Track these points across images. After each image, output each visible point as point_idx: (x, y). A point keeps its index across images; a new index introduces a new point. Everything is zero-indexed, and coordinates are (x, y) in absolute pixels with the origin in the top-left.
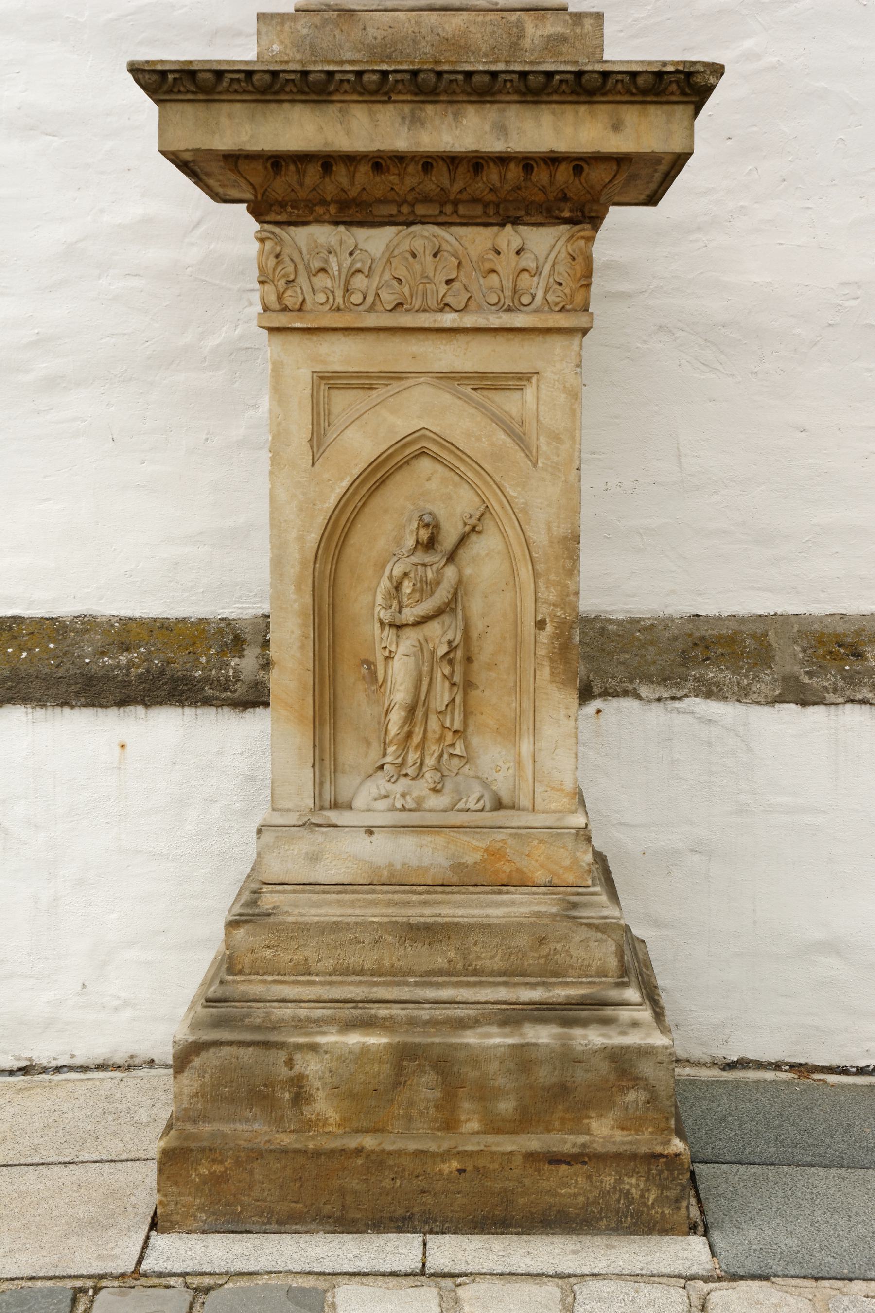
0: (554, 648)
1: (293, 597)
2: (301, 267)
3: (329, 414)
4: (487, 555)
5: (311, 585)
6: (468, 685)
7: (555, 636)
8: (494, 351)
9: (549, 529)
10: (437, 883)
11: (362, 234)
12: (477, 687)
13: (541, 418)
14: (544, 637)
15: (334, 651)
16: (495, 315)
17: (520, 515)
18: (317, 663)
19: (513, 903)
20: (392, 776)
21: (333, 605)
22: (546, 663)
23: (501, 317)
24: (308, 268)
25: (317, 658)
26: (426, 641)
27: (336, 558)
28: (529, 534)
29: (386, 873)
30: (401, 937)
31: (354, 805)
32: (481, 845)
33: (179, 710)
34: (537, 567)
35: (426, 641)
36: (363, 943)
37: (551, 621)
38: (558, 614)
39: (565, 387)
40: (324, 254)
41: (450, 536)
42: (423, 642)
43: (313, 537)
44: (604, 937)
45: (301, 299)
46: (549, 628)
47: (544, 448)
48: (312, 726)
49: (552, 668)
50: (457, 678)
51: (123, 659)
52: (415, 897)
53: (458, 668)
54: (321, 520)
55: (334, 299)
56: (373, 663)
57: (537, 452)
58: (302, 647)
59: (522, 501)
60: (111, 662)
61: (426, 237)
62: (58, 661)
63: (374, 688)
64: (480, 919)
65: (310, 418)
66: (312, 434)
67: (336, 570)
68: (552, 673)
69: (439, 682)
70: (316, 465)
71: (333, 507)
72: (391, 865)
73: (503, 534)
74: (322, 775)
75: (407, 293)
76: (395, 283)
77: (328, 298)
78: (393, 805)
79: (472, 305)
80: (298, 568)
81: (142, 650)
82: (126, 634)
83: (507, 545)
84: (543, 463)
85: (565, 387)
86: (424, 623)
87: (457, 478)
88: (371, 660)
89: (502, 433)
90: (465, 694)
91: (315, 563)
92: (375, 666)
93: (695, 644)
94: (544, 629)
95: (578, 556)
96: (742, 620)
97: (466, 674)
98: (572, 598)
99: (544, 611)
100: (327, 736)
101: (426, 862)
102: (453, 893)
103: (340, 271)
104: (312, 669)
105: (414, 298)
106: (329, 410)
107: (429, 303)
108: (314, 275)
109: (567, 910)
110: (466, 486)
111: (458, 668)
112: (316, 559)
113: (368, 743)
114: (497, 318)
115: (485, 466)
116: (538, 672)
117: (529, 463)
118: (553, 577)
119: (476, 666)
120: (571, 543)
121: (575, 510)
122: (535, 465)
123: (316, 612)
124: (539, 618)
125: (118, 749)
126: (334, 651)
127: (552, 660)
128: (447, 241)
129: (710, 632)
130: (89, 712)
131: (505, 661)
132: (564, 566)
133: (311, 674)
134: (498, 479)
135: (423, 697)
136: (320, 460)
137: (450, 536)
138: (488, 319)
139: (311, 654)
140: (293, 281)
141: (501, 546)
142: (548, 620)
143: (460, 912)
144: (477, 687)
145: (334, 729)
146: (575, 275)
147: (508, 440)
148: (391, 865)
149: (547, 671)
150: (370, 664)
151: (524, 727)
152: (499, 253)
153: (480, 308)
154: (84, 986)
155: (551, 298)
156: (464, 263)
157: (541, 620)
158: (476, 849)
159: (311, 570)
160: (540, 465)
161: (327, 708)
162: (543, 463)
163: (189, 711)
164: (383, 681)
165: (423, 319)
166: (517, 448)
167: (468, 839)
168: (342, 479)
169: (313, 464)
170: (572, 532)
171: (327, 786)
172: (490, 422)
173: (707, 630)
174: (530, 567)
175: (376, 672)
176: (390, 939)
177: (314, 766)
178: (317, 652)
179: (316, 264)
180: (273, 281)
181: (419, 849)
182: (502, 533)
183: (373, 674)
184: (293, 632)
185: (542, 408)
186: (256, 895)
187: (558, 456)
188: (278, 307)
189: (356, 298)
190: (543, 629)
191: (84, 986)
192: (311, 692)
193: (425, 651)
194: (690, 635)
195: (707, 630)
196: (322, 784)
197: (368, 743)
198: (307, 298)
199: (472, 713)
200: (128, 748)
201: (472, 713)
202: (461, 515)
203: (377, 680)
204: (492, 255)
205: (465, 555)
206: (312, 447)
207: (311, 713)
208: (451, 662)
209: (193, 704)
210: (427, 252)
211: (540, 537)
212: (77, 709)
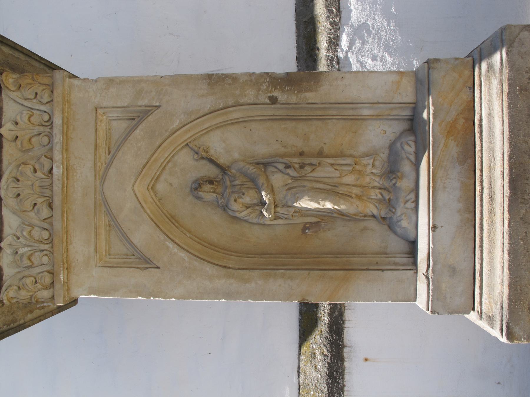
0: (291, 89)
1: (253, 285)
2: (26, 273)
3: (127, 255)
4: (224, 142)
5: (245, 271)
6: (320, 154)
7: (282, 90)
8: (81, 139)
9: (202, 96)
10: (473, 175)
11: (7, 230)
12: (322, 148)
13: (126, 104)
14: (281, 97)
15: (295, 254)
16: (54, 138)
17: (193, 117)
18: (303, 267)
19: (490, 115)
20: (390, 210)
21: (262, 254)
22: (303, 95)
23: (56, 134)
24: (27, 268)
25: (300, 267)
26: (286, 185)
27: (227, 252)
28: (206, 110)
29: (466, 215)
30: (521, 203)
31: (412, 238)
32: (443, 141)
33: (346, 330)
34: (230, 103)
35: (286, 185)
36: (526, 233)
37: (270, 93)
38: (265, 87)
39: (105, 89)
40: (18, 257)
41: (211, 171)
42: (286, 188)
43: (209, 269)
44: (517, 40)
45: (47, 273)
46: (276, 94)
47: (146, 102)
48: (351, 272)
49: (306, 91)
50: (314, 161)
51: (319, 357)
52: (486, 192)
53: (308, 160)
54: (197, 263)
55: (47, 250)
56: (305, 225)
57: (149, 106)
58: (291, 278)
59: (182, 116)
60: (320, 364)
61: (7, 187)
62: (320, 391)
63: (323, 225)
64: (505, 139)
65: (126, 269)
66: (137, 268)
67: (236, 252)
68: (310, 91)
69: (319, 173)
70: (159, 266)
71: (188, 254)
72: (459, 211)
73: (209, 130)
74: (389, 264)
75: (43, 199)
76: (36, 207)
77: (46, 255)
78: (412, 209)
79: (49, 155)
80: (232, 281)
81: (314, 347)
82: (307, 353)
83: (217, 127)
84: (156, 102)
85: (105, 89)
86: (272, 187)
87: (170, 165)
88: (301, 226)
89: (135, 132)
90: (327, 156)
91: (229, 268)
92: (306, 223)
93: (310, 56)
94: (276, 97)
95: (223, 74)
96: (298, 36)
97: (312, 156)
98: (253, 78)
99: (263, 98)
100: (359, 259)
101: (457, 184)
102: (482, 162)
103: (28, 246)
104: (307, 272)
105: (45, 195)
106: (124, 255)
107: (47, 184)
108: (32, 264)
109: (494, 72)
110: (176, 158)
111: (308, 160)
112: (225, 267)
113: (365, 229)
114: (56, 136)
115: (158, 144)
116: (310, 101)
117: (156, 111)
118: (238, 92)
119: (306, 149)
120: (214, 80)
121: (189, 78)
122: (158, 107)
123: (265, 267)
124: (268, 101)
125: (367, 363)
126: (295, 254)
127: (301, 91)
128: (10, 173)
129: (304, 50)
130: (347, 377)
131: (302, 127)
132: (230, 84)
133: (312, 272)
134: (167, 134)
135: (329, 187)
136: (154, 262)
137: (211, 171)
138: (57, 143)
139: (297, 272)
140: (36, 279)
141: (218, 132)
142: (270, 95)
143: (498, 156)
144: (322, 148)
145: (354, 254)
146: (30, 84)
147: (140, 127)
148: (459, 211)
149: (308, 95)
150: (305, 228)
151: (351, 112)
152: (17, 137)
153: (51, 149)
154: (499, 383)
155: (46, 99)
156: (23, 161)
157: (270, 100)
158: (446, 145)
159: (233, 271)
160: (157, 104)
161: (338, 260)
162: (156, 102)
163: (347, 324)
164: (113, 151)
165: (57, 188)
166: (145, 121)
167: (439, 151)
168: (168, 247)
169: (158, 268)
170: (205, 79)
171: (397, 260)
172: (128, 141)
173: (303, 52)
174: (231, 109)
175: (311, 223)
176: (523, 211)
177: (383, 270)
178: (295, 267)
179: (26, 262)
180: (35, 292)
181: (447, 190)
182: (209, 131)
183: (313, 225)
184: (280, 285)
185: (119, 105)
186: (484, 316)
187: (152, 91)
188: (51, 290)
189: (46, 235)
190: (276, 98)
191: (499, 383)
192: (326, 272)
193: (293, 186)
194: (306, 60)
195: (303, 52)
196: (395, 264)
197: (365, 229)
198: (45, 269)
199: (341, 152)
200: (368, 357)
201: (341, 152)
202: (197, 160)
203: (319, 222)
204: (18, 142)
205: (223, 161)
206: (147, 268)
207: (341, 272)
208: (302, 166)
209: (343, 322)
210: (16, 186)
211: (208, 103)
212: (345, 383)
